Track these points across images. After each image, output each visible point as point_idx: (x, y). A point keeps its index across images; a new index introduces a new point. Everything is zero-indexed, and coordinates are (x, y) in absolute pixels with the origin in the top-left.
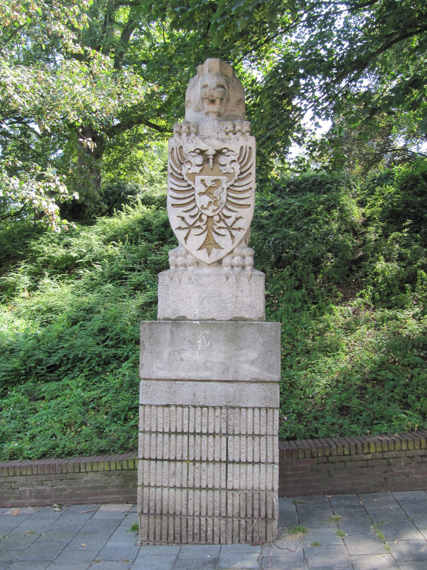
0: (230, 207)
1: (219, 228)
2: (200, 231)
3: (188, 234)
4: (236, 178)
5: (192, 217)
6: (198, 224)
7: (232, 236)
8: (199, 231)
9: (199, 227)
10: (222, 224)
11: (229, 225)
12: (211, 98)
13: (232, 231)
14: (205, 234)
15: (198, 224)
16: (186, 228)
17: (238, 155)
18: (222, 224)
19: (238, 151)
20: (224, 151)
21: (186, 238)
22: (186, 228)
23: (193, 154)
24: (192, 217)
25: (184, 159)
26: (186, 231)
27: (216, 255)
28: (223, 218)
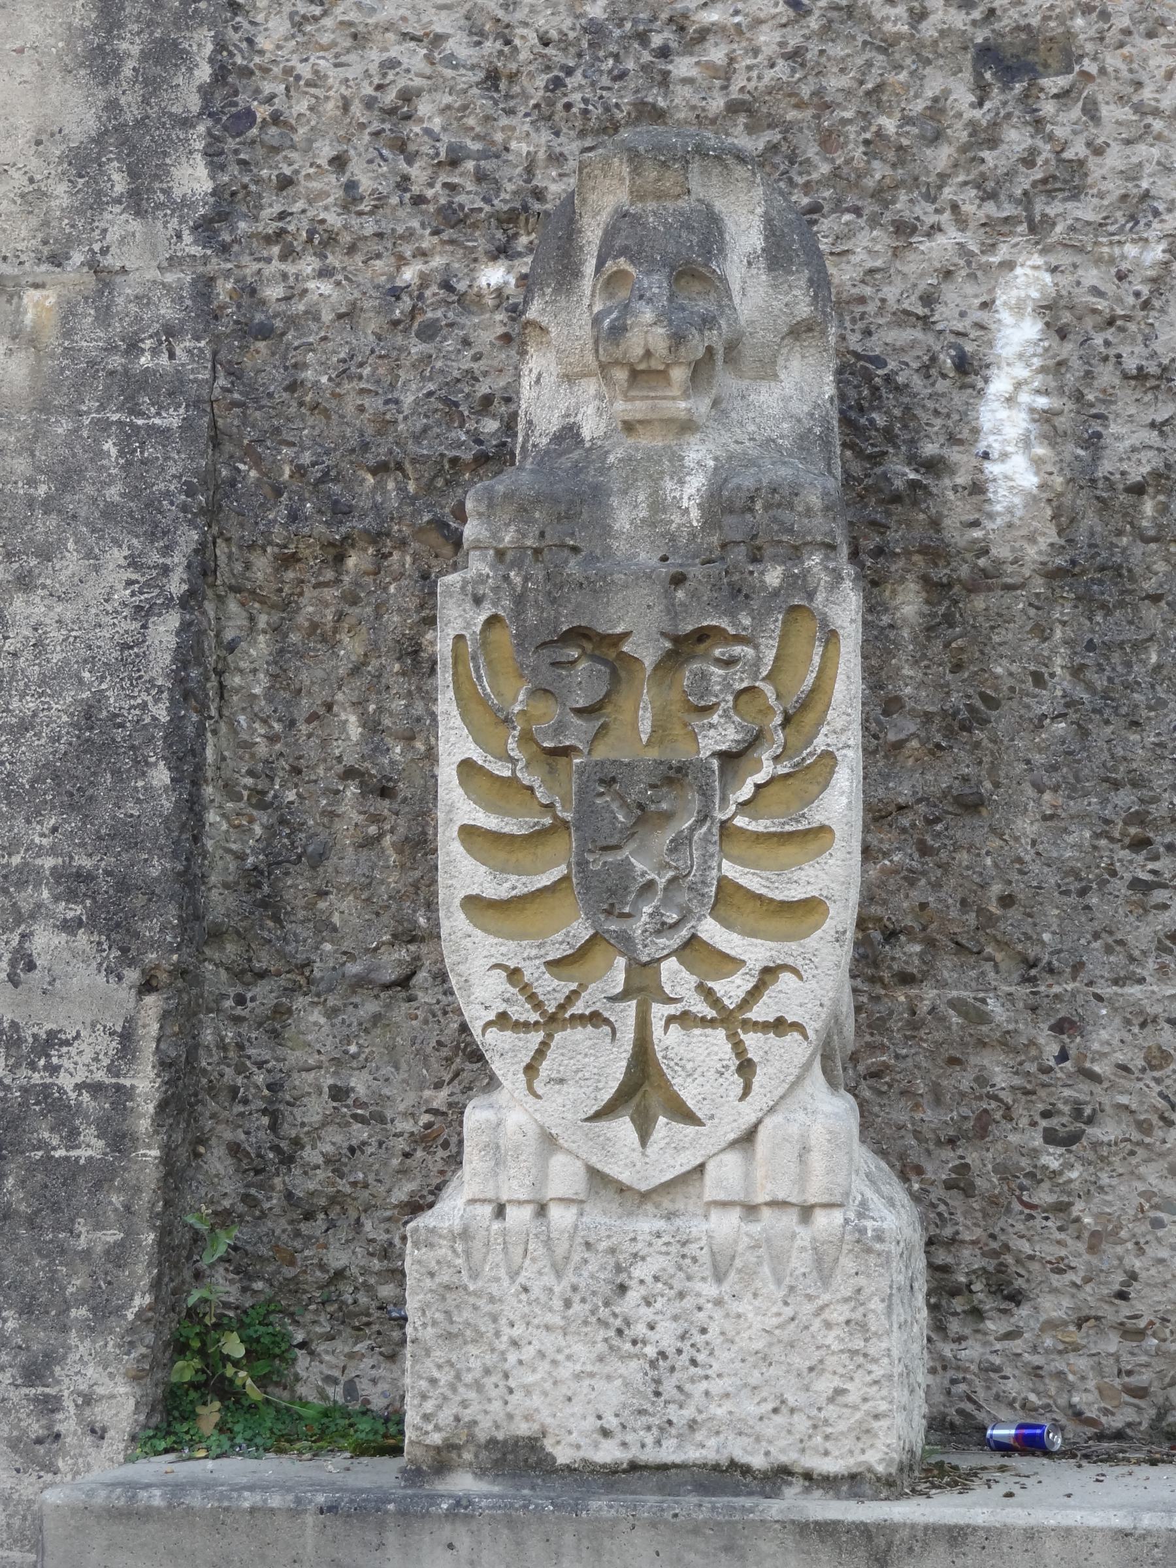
7: (746, 1067)
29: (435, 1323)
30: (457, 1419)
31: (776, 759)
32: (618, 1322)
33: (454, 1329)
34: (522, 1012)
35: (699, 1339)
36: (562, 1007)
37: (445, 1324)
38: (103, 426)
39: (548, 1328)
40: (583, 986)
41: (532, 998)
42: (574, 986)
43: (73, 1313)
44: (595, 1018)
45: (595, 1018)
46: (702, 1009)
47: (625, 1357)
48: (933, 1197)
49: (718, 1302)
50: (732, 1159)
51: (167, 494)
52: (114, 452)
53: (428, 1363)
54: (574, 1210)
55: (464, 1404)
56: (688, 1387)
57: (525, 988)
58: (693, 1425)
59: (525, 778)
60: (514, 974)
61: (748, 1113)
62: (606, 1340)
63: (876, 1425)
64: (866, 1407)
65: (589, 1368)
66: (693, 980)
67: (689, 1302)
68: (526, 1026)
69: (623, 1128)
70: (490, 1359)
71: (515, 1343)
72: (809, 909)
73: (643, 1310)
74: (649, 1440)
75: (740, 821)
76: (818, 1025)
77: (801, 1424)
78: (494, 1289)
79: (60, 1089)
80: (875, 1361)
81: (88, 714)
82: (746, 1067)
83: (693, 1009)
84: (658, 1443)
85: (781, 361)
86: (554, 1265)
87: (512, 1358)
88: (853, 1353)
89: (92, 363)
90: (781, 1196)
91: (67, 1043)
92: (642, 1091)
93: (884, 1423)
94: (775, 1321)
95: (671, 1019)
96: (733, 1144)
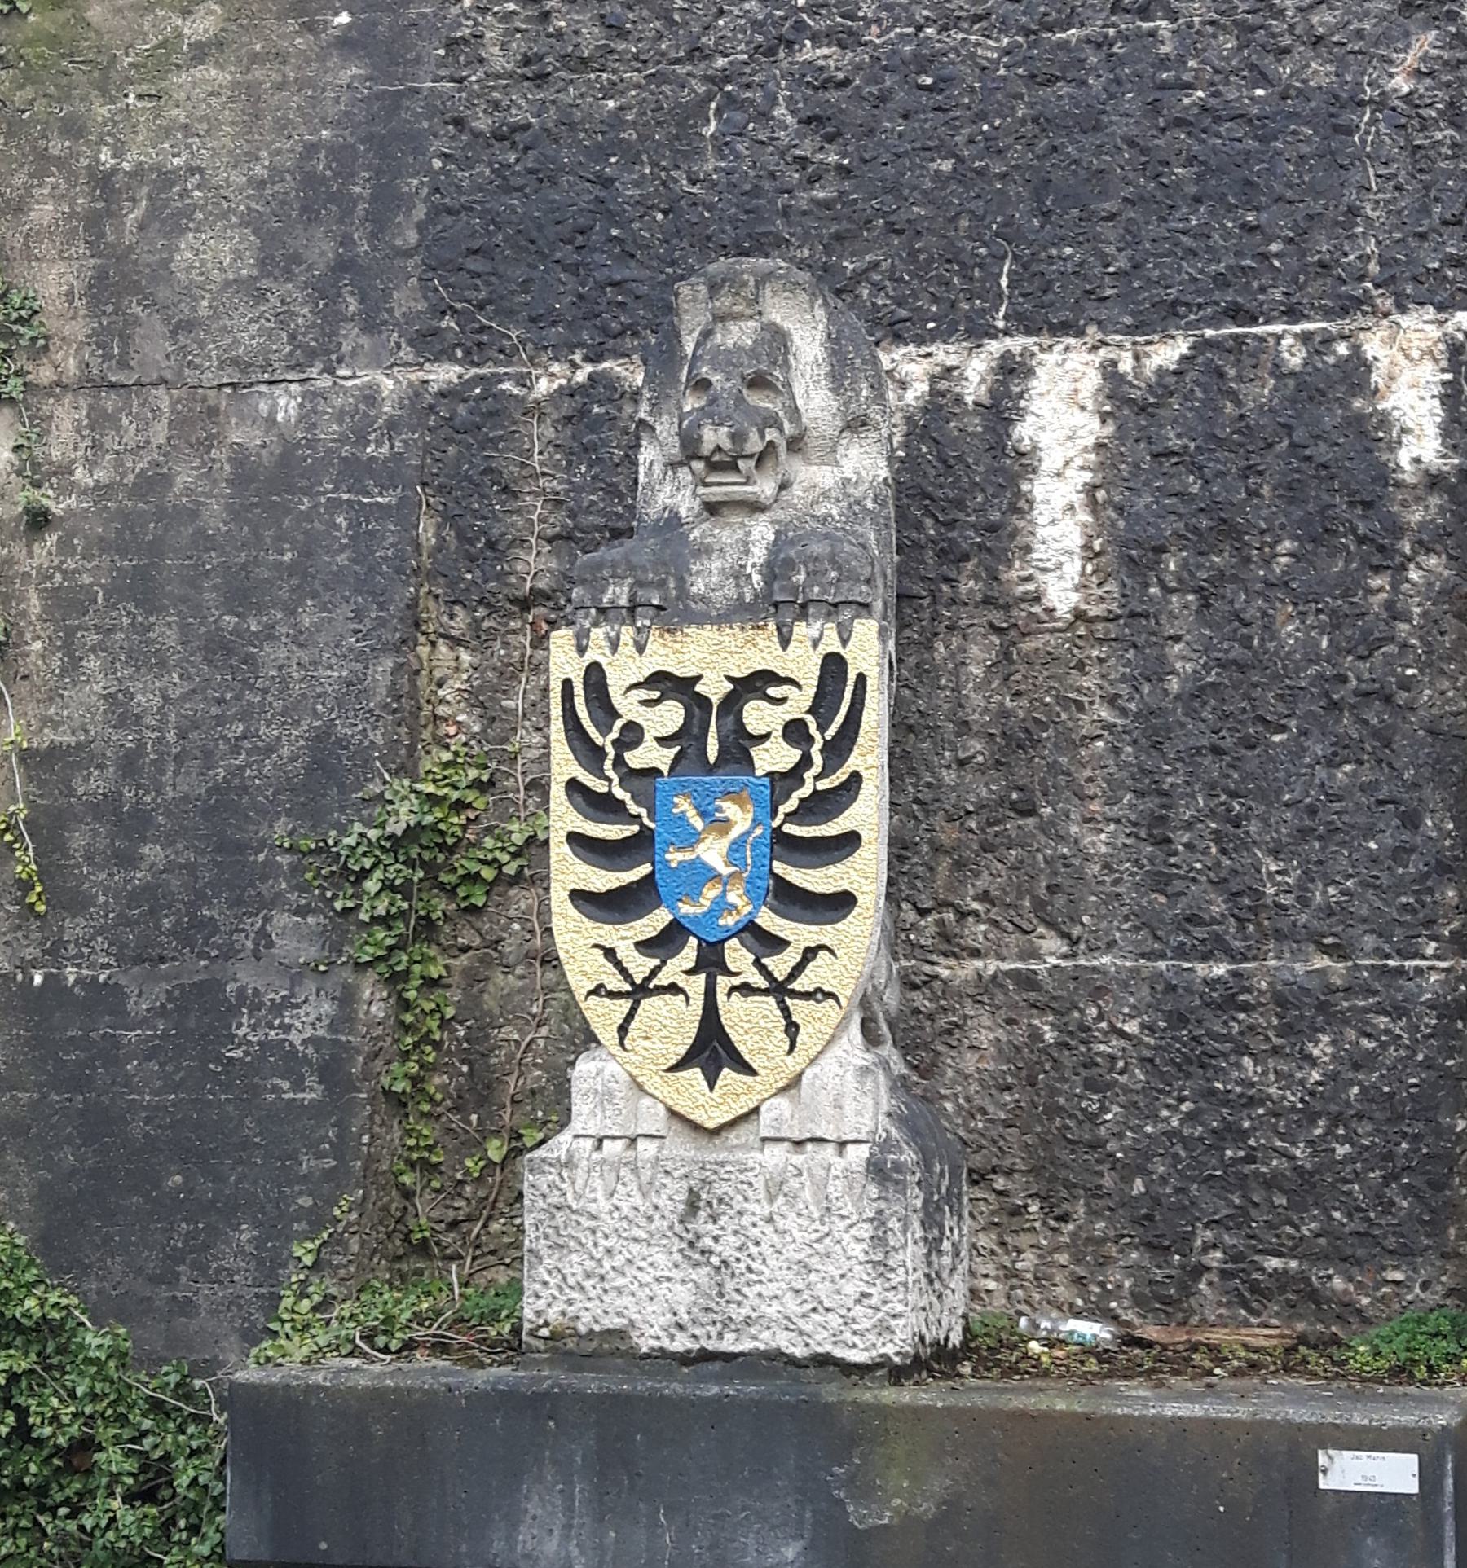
3: (630, 1016)
7: (792, 1029)
29: (546, 1237)
30: (563, 1314)
31: (817, 778)
32: (690, 1236)
33: (561, 1241)
34: (617, 983)
35: (754, 1250)
36: (648, 979)
37: (554, 1237)
38: (335, 505)
39: (636, 1240)
40: (664, 962)
41: (623, 971)
42: (657, 962)
43: (296, 1226)
44: (674, 989)
45: (674, 989)
46: (760, 982)
47: (697, 1265)
48: (994, 1133)
49: (770, 1220)
50: (783, 1103)
51: (385, 559)
52: (344, 524)
53: (541, 1269)
54: (656, 1143)
55: (570, 1302)
56: (746, 1290)
57: (618, 964)
58: (748, 1321)
59: (619, 793)
60: (610, 953)
61: (794, 1063)
62: (681, 1251)
63: (893, 1323)
64: (886, 1308)
65: (667, 1273)
66: (752, 957)
67: (746, 1221)
68: (619, 995)
69: (695, 1075)
70: (590, 1265)
71: (609, 1251)
72: (841, 903)
73: (710, 1226)
74: (714, 1334)
75: (789, 828)
76: (849, 993)
77: (834, 1321)
78: (592, 1208)
79: (291, 1044)
80: (893, 1270)
81: (321, 738)
82: (792, 1029)
83: (750, 981)
84: (720, 1335)
85: (841, 450)
86: (640, 1188)
87: (607, 1265)
88: (875, 1264)
89: (329, 451)
90: (819, 1134)
91: (298, 1006)
92: (712, 1050)
93: (902, 1322)
94: (815, 1236)
95: (733, 989)
96: (783, 1090)
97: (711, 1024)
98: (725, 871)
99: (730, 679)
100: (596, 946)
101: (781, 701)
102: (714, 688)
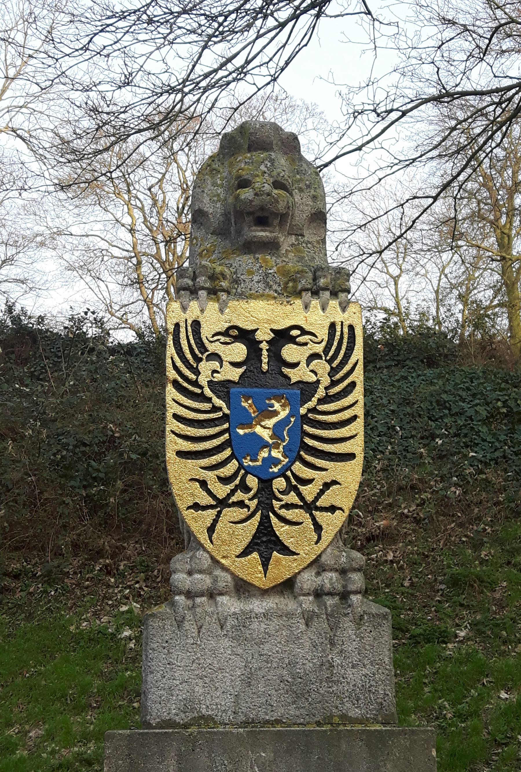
0: (309, 458)
1: (288, 506)
2: (243, 513)
3: (215, 521)
4: (321, 393)
5: (224, 480)
6: (239, 496)
7: (318, 528)
8: (241, 513)
9: (241, 504)
10: (292, 498)
11: (309, 498)
12: (259, 214)
13: (317, 514)
14: (258, 517)
15: (239, 496)
16: (212, 507)
17: (324, 344)
18: (292, 498)
19: (323, 334)
20: (295, 333)
21: (211, 530)
22: (212, 507)
23: (223, 339)
24: (224, 480)
25: (203, 348)
26: (214, 512)
27: (282, 567)
28: (294, 482)
34: (206, 500)
75: (328, 358)
97: (265, 528)
98: (271, 441)
99: (272, 330)
100: (191, 480)
101: (306, 344)
102: (264, 335)
